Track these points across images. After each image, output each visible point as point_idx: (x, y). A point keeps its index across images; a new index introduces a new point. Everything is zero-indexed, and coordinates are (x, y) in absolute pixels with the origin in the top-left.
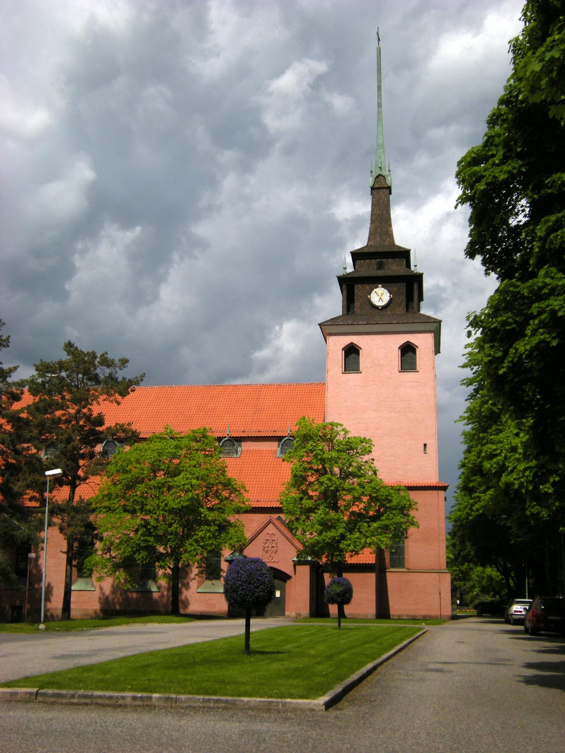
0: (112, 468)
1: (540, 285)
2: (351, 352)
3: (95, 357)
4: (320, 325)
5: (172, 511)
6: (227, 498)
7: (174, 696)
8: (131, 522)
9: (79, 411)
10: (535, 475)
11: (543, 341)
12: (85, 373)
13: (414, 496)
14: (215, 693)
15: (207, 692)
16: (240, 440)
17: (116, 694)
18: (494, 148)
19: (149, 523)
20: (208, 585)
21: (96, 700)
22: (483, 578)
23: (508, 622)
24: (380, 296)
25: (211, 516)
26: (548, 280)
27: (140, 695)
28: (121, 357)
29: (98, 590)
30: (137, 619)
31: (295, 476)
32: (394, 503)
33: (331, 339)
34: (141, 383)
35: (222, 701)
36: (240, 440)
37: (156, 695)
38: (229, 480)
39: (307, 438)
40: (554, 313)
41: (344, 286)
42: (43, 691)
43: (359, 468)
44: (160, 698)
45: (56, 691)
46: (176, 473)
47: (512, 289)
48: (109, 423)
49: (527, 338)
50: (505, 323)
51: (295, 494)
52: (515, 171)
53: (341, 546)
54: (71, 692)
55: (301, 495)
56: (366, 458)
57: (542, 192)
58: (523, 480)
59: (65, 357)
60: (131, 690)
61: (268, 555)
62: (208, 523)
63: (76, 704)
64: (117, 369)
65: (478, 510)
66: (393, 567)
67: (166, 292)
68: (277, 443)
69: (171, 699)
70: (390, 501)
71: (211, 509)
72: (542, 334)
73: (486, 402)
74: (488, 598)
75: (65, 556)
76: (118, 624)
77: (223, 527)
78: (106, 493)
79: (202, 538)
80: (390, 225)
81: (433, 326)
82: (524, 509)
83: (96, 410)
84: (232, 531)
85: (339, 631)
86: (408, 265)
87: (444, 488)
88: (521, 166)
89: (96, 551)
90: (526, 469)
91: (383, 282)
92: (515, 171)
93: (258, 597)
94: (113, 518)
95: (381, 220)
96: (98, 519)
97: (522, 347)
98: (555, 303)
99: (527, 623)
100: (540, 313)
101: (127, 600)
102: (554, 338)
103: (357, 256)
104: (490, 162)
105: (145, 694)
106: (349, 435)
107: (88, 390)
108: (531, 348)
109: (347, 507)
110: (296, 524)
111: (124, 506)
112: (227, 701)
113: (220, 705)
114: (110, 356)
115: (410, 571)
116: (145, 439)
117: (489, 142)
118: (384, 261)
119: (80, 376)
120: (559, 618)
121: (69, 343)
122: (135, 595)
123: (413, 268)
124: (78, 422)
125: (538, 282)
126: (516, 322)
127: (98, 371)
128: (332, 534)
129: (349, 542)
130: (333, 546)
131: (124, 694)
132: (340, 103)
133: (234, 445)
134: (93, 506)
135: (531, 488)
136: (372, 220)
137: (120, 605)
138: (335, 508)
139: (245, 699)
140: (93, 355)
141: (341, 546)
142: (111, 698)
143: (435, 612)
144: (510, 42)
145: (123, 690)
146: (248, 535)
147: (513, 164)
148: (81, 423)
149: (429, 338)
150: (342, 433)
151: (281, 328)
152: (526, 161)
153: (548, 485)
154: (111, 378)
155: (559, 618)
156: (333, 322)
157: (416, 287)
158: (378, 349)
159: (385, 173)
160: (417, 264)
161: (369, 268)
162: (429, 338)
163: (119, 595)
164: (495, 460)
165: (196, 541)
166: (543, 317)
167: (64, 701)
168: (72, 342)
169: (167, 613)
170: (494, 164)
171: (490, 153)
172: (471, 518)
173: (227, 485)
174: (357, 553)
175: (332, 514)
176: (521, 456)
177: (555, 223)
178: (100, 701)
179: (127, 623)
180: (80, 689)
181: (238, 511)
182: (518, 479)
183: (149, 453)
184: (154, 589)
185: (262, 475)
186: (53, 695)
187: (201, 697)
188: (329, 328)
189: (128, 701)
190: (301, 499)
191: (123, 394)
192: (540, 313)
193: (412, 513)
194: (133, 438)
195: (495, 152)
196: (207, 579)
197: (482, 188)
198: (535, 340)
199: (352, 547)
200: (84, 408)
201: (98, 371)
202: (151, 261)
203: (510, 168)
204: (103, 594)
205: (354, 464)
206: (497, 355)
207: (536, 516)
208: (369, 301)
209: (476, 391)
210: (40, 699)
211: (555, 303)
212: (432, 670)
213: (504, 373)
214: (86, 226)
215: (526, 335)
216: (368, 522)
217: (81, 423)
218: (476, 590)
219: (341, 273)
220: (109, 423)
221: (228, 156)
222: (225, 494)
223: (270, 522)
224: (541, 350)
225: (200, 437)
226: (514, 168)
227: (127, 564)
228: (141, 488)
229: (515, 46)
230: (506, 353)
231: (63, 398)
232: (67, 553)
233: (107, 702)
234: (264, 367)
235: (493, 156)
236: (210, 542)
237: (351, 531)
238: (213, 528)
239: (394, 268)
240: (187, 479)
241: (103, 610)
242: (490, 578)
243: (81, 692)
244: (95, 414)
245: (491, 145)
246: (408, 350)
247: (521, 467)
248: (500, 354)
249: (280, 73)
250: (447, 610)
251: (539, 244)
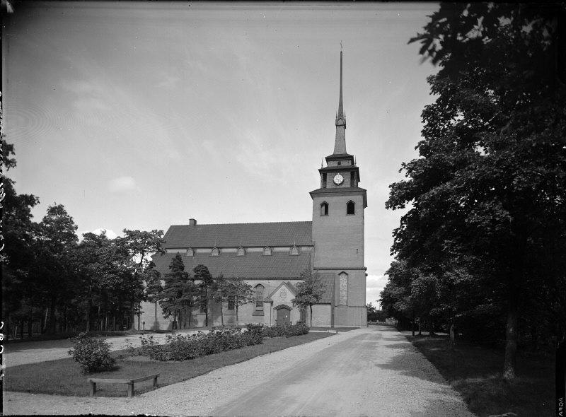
24: (338, 178)
95: (340, 139)
103: (328, 159)
161: (334, 164)
239: (345, 164)
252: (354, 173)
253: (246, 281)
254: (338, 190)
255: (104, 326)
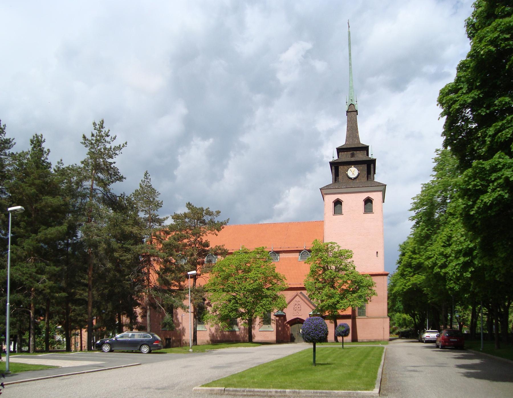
0: (215, 269)
1: (496, 163)
2: (338, 203)
3: (203, 211)
4: (320, 189)
5: (248, 291)
6: (275, 283)
7: (297, 390)
8: (225, 296)
9: (196, 240)
10: (462, 267)
11: (500, 195)
12: (199, 219)
13: (375, 279)
14: (318, 389)
15: (314, 388)
16: (278, 252)
17: (266, 390)
18: (461, 84)
19: (236, 298)
20: (266, 327)
21: (256, 393)
22: (400, 319)
23: (423, 342)
24: (353, 172)
25: (269, 293)
26: (501, 160)
27: (279, 390)
28: (217, 210)
29: (208, 331)
30: (232, 345)
31: (312, 271)
32: (365, 284)
33: (326, 197)
34: (227, 224)
35: (323, 393)
36: (278, 252)
37: (288, 390)
38: (277, 274)
39: (318, 250)
40: (507, 179)
41: (333, 167)
42: (228, 388)
43: (346, 266)
44: (290, 392)
45: (235, 389)
46: (249, 271)
47: (480, 166)
48: (212, 246)
49: (489, 194)
50: (475, 185)
51: (312, 280)
52: (476, 97)
53: (337, 306)
54: (243, 389)
55: (315, 281)
56: (349, 260)
57: (492, 109)
58: (454, 271)
59: (187, 210)
60: (273, 388)
61: (296, 312)
62: (266, 297)
63: (245, 395)
64: (215, 217)
65: (409, 286)
66: (359, 316)
67: (227, 174)
68: (298, 254)
69: (296, 392)
70: (362, 283)
71: (268, 289)
72: (499, 191)
73: (423, 229)
74: (403, 329)
75: (192, 314)
76: (223, 348)
77: (275, 298)
78: (213, 282)
79: (264, 305)
80: (358, 132)
81: (382, 188)
82: (445, 285)
83: (204, 239)
84: (279, 300)
85: (343, 350)
86: (368, 155)
87: (386, 275)
88: (480, 94)
89: (209, 311)
90: (456, 265)
91: (354, 164)
92: (476, 97)
93: (320, 337)
94: (217, 295)
95: (352, 129)
96: (209, 295)
97: (487, 198)
98: (508, 173)
99: (438, 342)
100: (496, 180)
101: (224, 336)
102: (506, 193)
103: (340, 150)
104: (460, 92)
105: (282, 390)
106: (340, 249)
107: (200, 228)
108: (493, 199)
109: (340, 286)
110: (313, 296)
111: (223, 289)
112: (326, 393)
113: (323, 395)
114: (211, 210)
115: (368, 318)
116: (231, 253)
117: (458, 80)
118: (355, 152)
119: (196, 221)
120: (456, 340)
121: (189, 203)
122: (227, 333)
123: (370, 156)
124: (195, 246)
125: (495, 161)
126: (481, 185)
127: (205, 218)
128: (333, 300)
129: (341, 305)
130: (333, 307)
131: (271, 390)
132: (319, 65)
133: (275, 255)
134: (206, 289)
135: (459, 275)
136: (347, 130)
137: (220, 337)
138: (333, 287)
139: (336, 391)
140: (202, 209)
141: (337, 306)
142: (264, 392)
143: (380, 338)
144: (465, 21)
145: (269, 388)
146: (287, 302)
147: (475, 93)
148: (197, 246)
149: (380, 194)
150: (337, 247)
151: (289, 191)
152: (482, 91)
153: (468, 273)
154: (212, 221)
155: (456, 340)
156: (328, 187)
157: (372, 166)
158: (353, 201)
159: (354, 103)
160: (373, 154)
161: (346, 157)
162: (380, 194)
163: (219, 333)
164: (431, 260)
165: (261, 306)
166: (499, 181)
167: (239, 393)
168: (191, 203)
169: (244, 342)
170: (463, 93)
171: (459, 87)
172: (405, 290)
173: (276, 277)
174: (345, 310)
175: (332, 290)
176: (453, 258)
177: (501, 126)
178: (258, 393)
179: (228, 347)
180: (246, 387)
181: (282, 290)
182: (452, 270)
183: (234, 260)
184: (237, 329)
185: (295, 271)
186: (233, 391)
187: (312, 391)
188: (325, 191)
189: (273, 393)
190: (315, 283)
191: (218, 230)
192: (496, 180)
193: (374, 288)
194: (225, 253)
195: (462, 86)
196: (264, 324)
197: (457, 107)
198: (495, 195)
199: (343, 307)
200: (198, 237)
201: (205, 218)
202: (219, 157)
203: (473, 95)
204: (211, 332)
205: (343, 264)
206: (469, 204)
207: (451, 289)
208: (347, 175)
209: (417, 223)
210: (226, 393)
211: (507, 173)
212: (411, 371)
213: (474, 213)
214: (183, 140)
215: (488, 192)
216: (351, 294)
217: (197, 246)
218: (396, 325)
219: (331, 160)
220: (212, 246)
221: (258, 97)
222: (275, 281)
223: (297, 295)
224: (499, 200)
225: (261, 252)
226: (475, 95)
227: (224, 318)
228: (232, 279)
229: (468, 23)
230: (474, 203)
231: (187, 233)
232: (194, 312)
233: (262, 394)
234: (280, 213)
235: (461, 88)
236: (268, 306)
237: (342, 299)
238: (270, 299)
239: (360, 156)
240: (256, 274)
241: (211, 340)
242: (404, 319)
243: (248, 389)
244: (204, 241)
245: (460, 82)
246: (368, 201)
247: (454, 264)
248: (471, 203)
249: (286, 49)
250: (387, 336)
251: (489, 139)
252: (369, 166)
253: (195, 388)
254: (352, 186)
255: (81, 347)
